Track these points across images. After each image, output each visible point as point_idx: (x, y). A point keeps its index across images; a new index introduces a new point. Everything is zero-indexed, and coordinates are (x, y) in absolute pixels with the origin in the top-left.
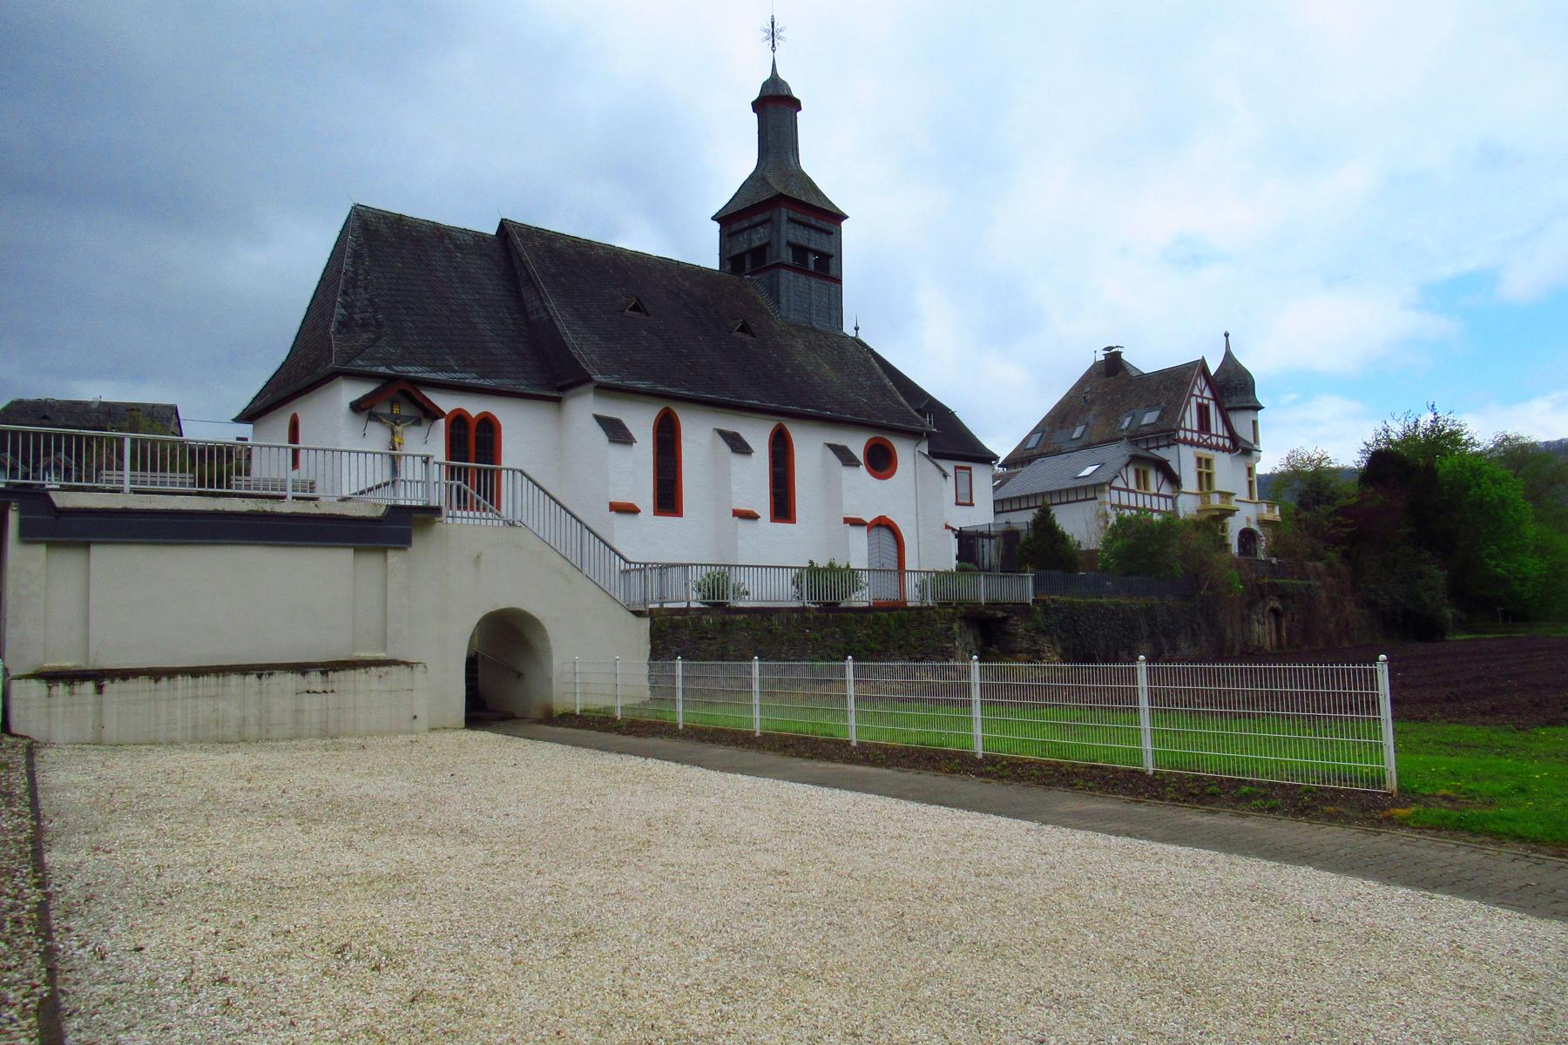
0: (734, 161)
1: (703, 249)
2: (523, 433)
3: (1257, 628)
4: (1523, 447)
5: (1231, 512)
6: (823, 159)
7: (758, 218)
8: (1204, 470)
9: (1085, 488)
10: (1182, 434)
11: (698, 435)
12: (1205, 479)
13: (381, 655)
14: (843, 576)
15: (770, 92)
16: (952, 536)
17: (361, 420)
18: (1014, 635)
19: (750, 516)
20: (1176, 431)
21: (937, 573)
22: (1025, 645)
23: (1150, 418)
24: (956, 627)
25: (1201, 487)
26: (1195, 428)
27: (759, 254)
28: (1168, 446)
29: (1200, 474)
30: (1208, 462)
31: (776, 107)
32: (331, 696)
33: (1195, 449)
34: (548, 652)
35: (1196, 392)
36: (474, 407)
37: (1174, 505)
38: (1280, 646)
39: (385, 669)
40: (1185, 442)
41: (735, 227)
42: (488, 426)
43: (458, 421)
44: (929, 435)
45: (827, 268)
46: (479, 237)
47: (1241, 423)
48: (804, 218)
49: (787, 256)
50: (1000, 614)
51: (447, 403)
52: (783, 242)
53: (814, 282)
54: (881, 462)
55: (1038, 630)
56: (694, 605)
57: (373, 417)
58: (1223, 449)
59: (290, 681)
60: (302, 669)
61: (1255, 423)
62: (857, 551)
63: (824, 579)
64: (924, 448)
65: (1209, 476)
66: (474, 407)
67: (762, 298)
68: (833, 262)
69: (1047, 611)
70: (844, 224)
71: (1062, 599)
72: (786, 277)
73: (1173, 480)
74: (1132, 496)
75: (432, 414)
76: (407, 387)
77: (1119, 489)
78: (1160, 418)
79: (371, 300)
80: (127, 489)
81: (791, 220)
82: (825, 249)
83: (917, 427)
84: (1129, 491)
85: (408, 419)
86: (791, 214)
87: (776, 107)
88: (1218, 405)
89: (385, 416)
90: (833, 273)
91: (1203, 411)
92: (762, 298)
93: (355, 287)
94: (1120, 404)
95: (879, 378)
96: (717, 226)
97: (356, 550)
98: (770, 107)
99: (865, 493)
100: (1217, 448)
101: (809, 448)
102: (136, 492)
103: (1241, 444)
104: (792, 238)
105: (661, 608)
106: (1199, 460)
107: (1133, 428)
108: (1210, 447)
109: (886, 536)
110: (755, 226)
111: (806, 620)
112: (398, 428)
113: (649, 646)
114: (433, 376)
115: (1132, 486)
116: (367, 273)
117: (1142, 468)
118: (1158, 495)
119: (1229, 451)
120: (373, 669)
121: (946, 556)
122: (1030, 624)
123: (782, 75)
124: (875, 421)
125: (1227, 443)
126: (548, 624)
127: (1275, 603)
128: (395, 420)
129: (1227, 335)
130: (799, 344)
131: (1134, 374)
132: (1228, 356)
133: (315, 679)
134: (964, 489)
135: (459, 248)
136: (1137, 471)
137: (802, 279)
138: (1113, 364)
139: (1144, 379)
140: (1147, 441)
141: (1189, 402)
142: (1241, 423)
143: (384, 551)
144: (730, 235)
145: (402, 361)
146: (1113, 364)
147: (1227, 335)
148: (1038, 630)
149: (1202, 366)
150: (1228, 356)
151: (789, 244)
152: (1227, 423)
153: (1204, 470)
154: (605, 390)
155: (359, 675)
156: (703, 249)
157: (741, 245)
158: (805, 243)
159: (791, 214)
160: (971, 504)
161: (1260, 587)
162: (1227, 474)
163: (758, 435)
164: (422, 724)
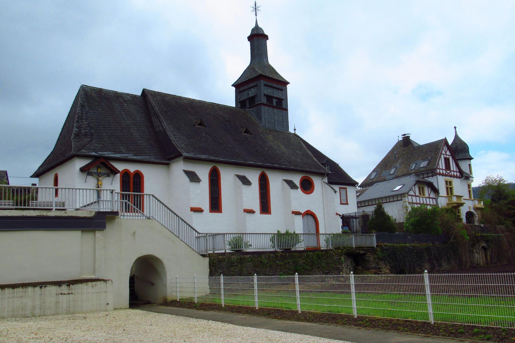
0: (239, 62)
1: (228, 98)
2: (153, 179)
3: (476, 255)
5: (462, 204)
6: (278, 59)
7: (251, 85)
8: (449, 186)
10: (438, 171)
11: (228, 177)
12: (450, 190)
13: (93, 277)
14: (294, 237)
15: (255, 32)
20: (436, 169)
21: (333, 234)
23: (424, 164)
24: (342, 258)
25: (448, 194)
26: (444, 168)
27: (252, 100)
28: (433, 176)
29: (447, 188)
30: (450, 183)
31: (258, 39)
33: (444, 177)
35: (443, 152)
36: (132, 168)
37: (437, 202)
39: (94, 283)
40: (440, 174)
41: (242, 89)
43: (126, 174)
44: (328, 175)
49: (264, 100)
50: (362, 252)
51: (120, 167)
53: (276, 111)
54: (307, 187)
57: (90, 174)
58: (457, 177)
59: (53, 289)
60: (59, 284)
61: (470, 165)
62: (298, 226)
63: (284, 238)
64: (326, 180)
66: (132, 168)
68: (284, 102)
69: (382, 250)
70: (288, 86)
72: (265, 110)
73: (436, 191)
75: (114, 172)
77: (412, 196)
78: (428, 164)
79: (88, 124)
81: (265, 85)
83: (322, 171)
84: (416, 196)
85: (104, 174)
86: (266, 83)
87: (258, 39)
89: (94, 173)
90: (284, 107)
91: (447, 160)
93: (82, 119)
94: (408, 157)
95: (305, 151)
96: (234, 89)
97: (82, 231)
98: (255, 39)
99: (301, 201)
100: (454, 176)
101: (276, 181)
103: (464, 175)
104: (266, 93)
105: (214, 253)
106: (446, 182)
107: (416, 168)
108: (451, 176)
109: (310, 219)
111: (277, 257)
112: (100, 178)
113: (209, 270)
114: (115, 155)
115: (417, 194)
116: (87, 113)
117: (421, 186)
118: (429, 198)
119: (460, 178)
120: (90, 283)
121: (337, 227)
122: (375, 256)
123: (260, 25)
125: (458, 174)
126: (165, 261)
127: (484, 244)
128: (99, 175)
129: (455, 128)
130: (270, 137)
132: (456, 136)
133: (64, 288)
136: (419, 188)
138: (406, 141)
139: (420, 147)
141: (440, 157)
143: (94, 231)
144: (240, 92)
146: (406, 141)
147: (455, 128)
148: (379, 258)
149: (445, 141)
151: (265, 95)
152: (457, 165)
153: (449, 186)
154: (187, 159)
155: (83, 286)
156: (228, 98)
158: (272, 95)
161: (477, 237)
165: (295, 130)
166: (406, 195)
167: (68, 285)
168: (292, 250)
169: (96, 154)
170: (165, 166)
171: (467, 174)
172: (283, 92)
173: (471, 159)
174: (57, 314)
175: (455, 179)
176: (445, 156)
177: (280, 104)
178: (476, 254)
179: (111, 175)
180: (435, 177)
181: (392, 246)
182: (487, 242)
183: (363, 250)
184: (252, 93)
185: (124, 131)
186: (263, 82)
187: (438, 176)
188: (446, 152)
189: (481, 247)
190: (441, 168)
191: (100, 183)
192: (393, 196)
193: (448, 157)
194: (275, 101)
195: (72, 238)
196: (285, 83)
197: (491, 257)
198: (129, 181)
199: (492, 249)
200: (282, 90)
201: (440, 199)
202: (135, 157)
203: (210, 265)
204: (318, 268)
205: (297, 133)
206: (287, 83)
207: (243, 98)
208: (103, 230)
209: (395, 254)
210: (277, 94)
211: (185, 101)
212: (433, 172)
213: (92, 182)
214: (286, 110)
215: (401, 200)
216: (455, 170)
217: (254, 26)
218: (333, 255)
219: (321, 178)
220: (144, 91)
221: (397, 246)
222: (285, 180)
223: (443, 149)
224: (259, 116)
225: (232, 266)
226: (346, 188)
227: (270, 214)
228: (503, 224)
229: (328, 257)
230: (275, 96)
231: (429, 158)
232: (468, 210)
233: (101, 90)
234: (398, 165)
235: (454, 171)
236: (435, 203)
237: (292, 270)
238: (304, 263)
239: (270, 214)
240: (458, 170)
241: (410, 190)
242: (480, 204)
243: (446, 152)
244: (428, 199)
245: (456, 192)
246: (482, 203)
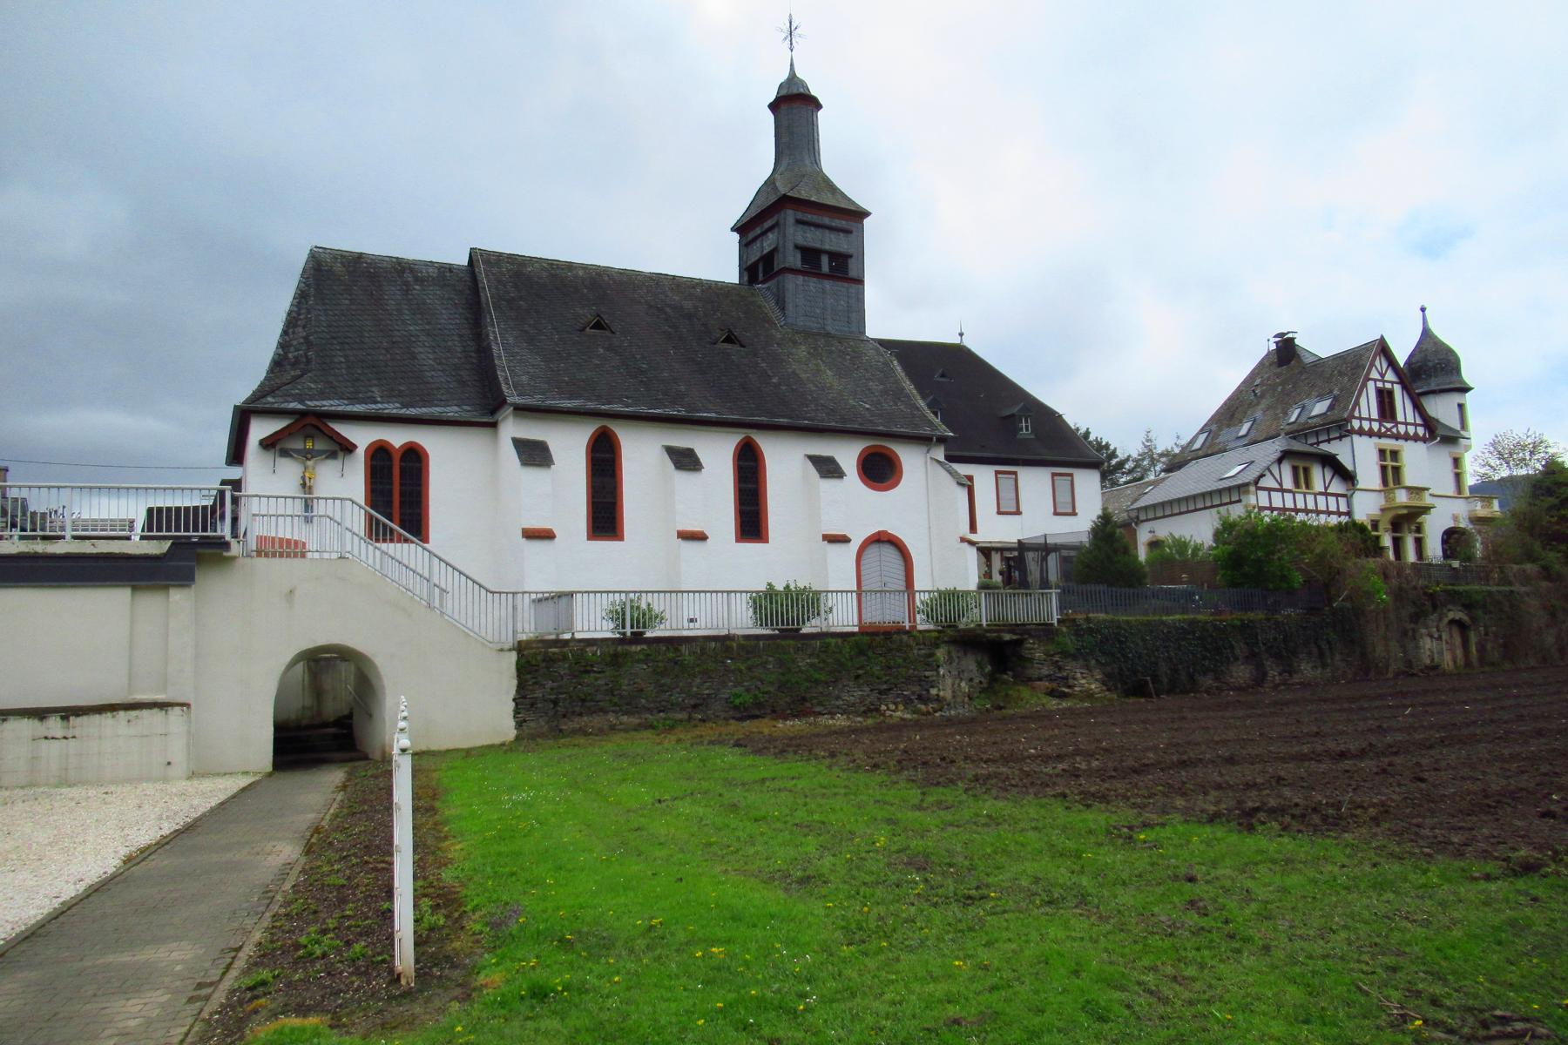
0: (754, 162)
1: (719, 262)
2: (456, 465)
3: (1427, 644)
4: (374, 681)
5: (1426, 510)
6: (842, 156)
8: (1389, 463)
9: (1229, 489)
10: (1356, 424)
11: (641, 454)
12: (1391, 473)
13: (160, 697)
14: (808, 601)
15: (784, 92)
16: (974, 550)
17: (268, 457)
18: (1031, 660)
20: (1348, 420)
21: (939, 592)
22: (1045, 671)
23: (1320, 408)
24: (941, 653)
25: (1385, 482)
26: (1375, 415)
27: (768, 259)
28: (1340, 438)
29: (1384, 469)
30: (1395, 454)
31: (794, 107)
32: (72, 742)
33: (1375, 440)
35: (1374, 375)
36: (397, 437)
37: (1349, 504)
38: (1468, 664)
39: (133, 713)
40: (1361, 432)
41: (751, 235)
42: (415, 458)
43: (379, 454)
44: (942, 440)
46: (446, 270)
47: (1442, 409)
48: (809, 217)
49: (794, 260)
50: (1007, 637)
51: (362, 437)
52: (790, 246)
53: (828, 284)
54: (879, 471)
55: (1065, 654)
56: (922, 626)
57: (285, 453)
58: (1416, 438)
59: (27, 726)
60: (40, 714)
61: (1461, 406)
62: (836, 573)
63: (784, 608)
64: (939, 453)
65: (1397, 471)
66: (397, 437)
67: (769, 306)
68: (852, 263)
69: (1078, 632)
70: (866, 221)
71: (1102, 616)
72: (793, 283)
73: (1348, 477)
74: (1288, 497)
75: (348, 448)
76: (314, 421)
77: (1269, 490)
78: (1331, 407)
79: (306, 338)
80: (68, 537)
81: (799, 222)
83: (927, 431)
84: (1283, 491)
86: (800, 216)
87: (794, 107)
88: (1405, 388)
89: (298, 451)
90: (853, 274)
91: (1385, 398)
92: (769, 306)
93: (296, 326)
94: (1298, 396)
95: (897, 382)
96: (736, 236)
97: (134, 588)
98: (784, 107)
99: (854, 505)
100: (1406, 437)
101: (785, 462)
102: (75, 538)
103: (1440, 432)
104: (800, 241)
105: (573, 639)
106: (1382, 452)
107: (1302, 420)
108: (1397, 437)
109: (889, 553)
110: (764, 233)
111: (728, 649)
112: (309, 463)
113: (515, 682)
114: (349, 408)
115: (1288, 483)
116: (309, 312)
117: (1301, 464)
118: (1326, 494)
119: (1424, 440)
120: (122, 713)
121: (966, 574)
122: (1051, 648)
124: (871, 428)
125: (1421, 431)
126: (379, 661)
127: (1457, 614)
128: (307, 455)
129: (1423, 310)
130: (802, 351)
131: (1308, 360)
132: (1426, 333)
133: (54, 725)
134: (1064, 497)
135: (418, 280)
136: (1295, 470)
137: (813, 284)
138: (1286, 350)
139: (1320, 363)
140: (1317, 434)
141: (1364, 385)
142: (1442, 409)
143: (167, 587)
145: (322, 395)
146: (1286, 350)
147: (1423, 310)
148: (1065, 654)
149: (1383, 349)
150: (1426, 333)
151: (797, 247)
152: (1418, 407)
153: (1389, 463)
154: (523, 411)
155: (106, 720)
156: (719, 262)
158: (818, 245)
159: (800, 216)
160: (1018, 512)
161: (1432, 596)
162: (1422, 465)
163: (717, 453)
164: (180, 768)
165: (961, 335)
166: (1252, 488)
167: (65, 718)
168: (804, 631)
169: (300, 407)
170: (487, 431)
171: (1451, 429)
172: (852, 237)
173: (1465, 389)
174: (31, 785)
175: (1410, 443)
176: (1380, 385)
177: (843, 270)
178: (1428, 640)
179: (341, 454)
180: (1346, 440)
181: (1112, 621)
182: (1468, 607)
183: (1012, 632)
186: (790, 215)
187: (1356, 438)
188: (1383, 375)
189: (1446, 621)
190: (1365, 414)
192: (1220, 492)
193: (1388, 386)
194: (825, 260)
195: (105, 607)
196: (859, 214)
197: (1482, 649)
198: (390, 468)
199: (1486, 627)
200: (848, 232)
201: (1358, 498)
202: (402, 411)
203: (518, 670)
204: (858, 677)
206: (866, 214)
207: (753, 259)
208: (188, 586)
209: (1121, 642)
211: (581, 273)
212: (1339, 426)
213: (288, 474)
214: (860, 281)
215: (1239, 501)
216: (1410, 419)
217: (784, 76)
218: (908, 646)
219: (924, 449)
221: (1128, 622)
222: (811, 458)
223: (1372, 364)
224: (781, 304)
225: (587, 672)
226: (1071, 475)
227: (767, 541)
228: (1534, 561)
229: (890, 650)
230: (827, 247)
231: (1336, 392)
232: (1451, 524)
233: (360, 257)
234: (1259, 414)
235: (1406, 424)
236: (1343, 508)
237: (772, 683)
238: (812, 665)
239: (767, 541)
240: (1419, 421)
241: (1262, 476)
242: (1490, 505)
243: (1383, 375)
244: (1321, 499)
245: (1409, 478)
246: (1496, 505)
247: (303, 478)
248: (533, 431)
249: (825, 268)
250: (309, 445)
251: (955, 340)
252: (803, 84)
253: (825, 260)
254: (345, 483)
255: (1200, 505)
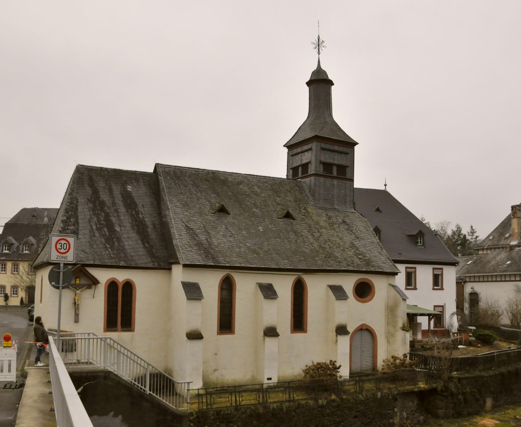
0: (296, 112)
1: (278, 168)
6: (344, 115)
7: (305, 147)
19: (271, 332)
27: (305, 166)
31: (320, 85)
34: (356, 282)
36: (121, 276)
41: (295, 151)
43: (112, 285)
45: (344, 174)
51: (104, 276)
53: (335, 182)
63: (320, 378)
66: (121, 276)
68: (348, 170)
70: (356, 148)
75: (95, 282)
82: (343, 163)
86: (323, 145)
87: (320, 85)
96: (286, 150)
99: (353, 312)
109: (366, 336)
112: (78, 292)
123: (323, 67)
128: (77, 287)
137: (328, 181)
144: (292, 156)
156: (278, 168)
157: (298, 161)
158: (331, 161)
159: (323, 145)
165: (385, 185)
184: (306, 158)
185: (127, 218)
191: (77, 298)
194: (335, 169)
200: (347, 154)
205: (389, 190)
206: (356, 144)
210: (338, 159)
213: (68, 295)
217: (315, 67)
220: (157, 166)
227: (306, 332)
230: (336, 162)
239: (306, 332)
247: (75, 299)
248: (193, 277)
249: (335, 173)
250: (78, 282)
251: (383, 188)
252: (325, 73)
253: (335, 169)
254: (95, 304)
255: (508, 279)
